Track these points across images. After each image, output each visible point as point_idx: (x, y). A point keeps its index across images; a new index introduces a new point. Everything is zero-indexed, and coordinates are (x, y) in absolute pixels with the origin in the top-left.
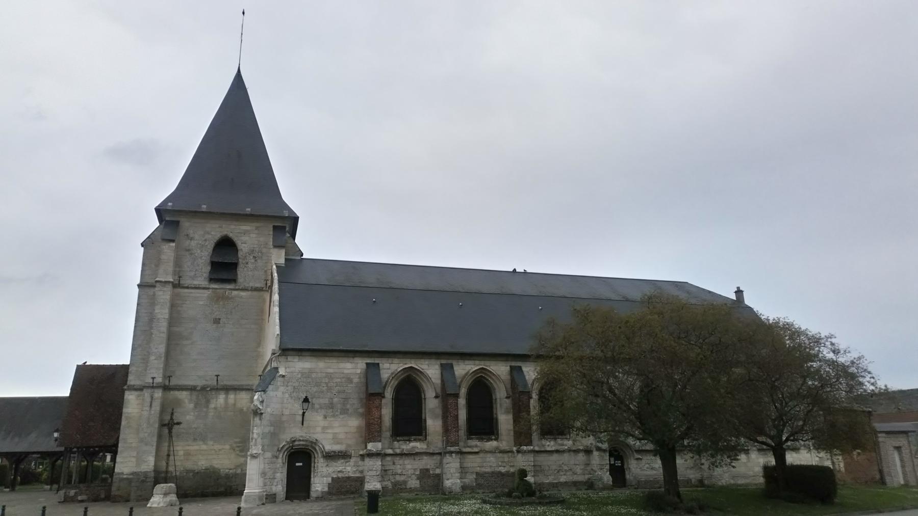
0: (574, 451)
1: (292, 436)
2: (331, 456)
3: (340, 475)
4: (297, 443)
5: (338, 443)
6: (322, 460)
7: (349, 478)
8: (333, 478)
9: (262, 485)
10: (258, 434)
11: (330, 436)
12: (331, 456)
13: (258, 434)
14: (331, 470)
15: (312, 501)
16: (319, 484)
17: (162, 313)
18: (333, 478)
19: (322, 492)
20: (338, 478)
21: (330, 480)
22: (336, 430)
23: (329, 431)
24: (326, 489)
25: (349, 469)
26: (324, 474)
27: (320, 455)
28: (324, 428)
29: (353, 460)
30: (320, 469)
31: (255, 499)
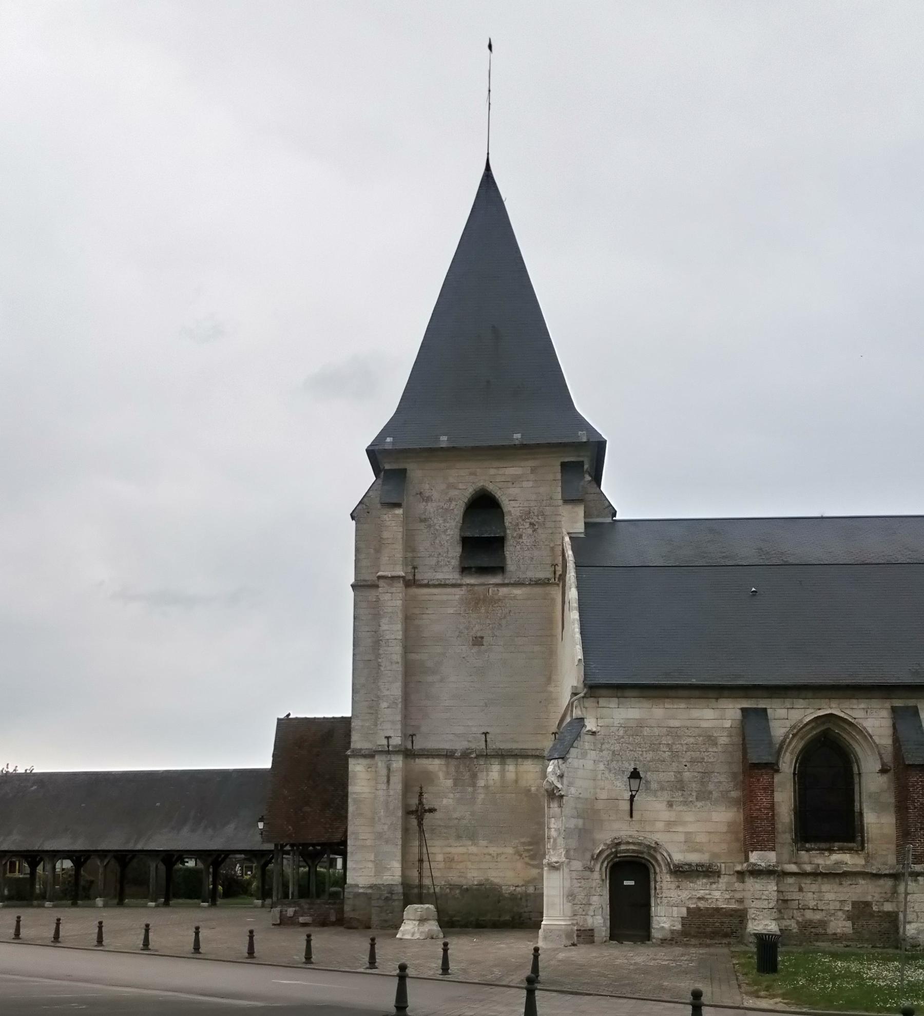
2: (683, 872)
3: (702, 904)
4: (623, 847)
6: (667, 878)
7: (718, 910)
8: (688, 909)
10: (558, 830)
11: (682, 838)
12: (683, 872)
14: (685, 895)
15: (654, 945)
16: (666, 916)
18: (688, 909)
20: (699, 909)
21: (684, 911)
24: (678, 927)
25: (717, 894)
27: (664, 870)
28: (669, 823)
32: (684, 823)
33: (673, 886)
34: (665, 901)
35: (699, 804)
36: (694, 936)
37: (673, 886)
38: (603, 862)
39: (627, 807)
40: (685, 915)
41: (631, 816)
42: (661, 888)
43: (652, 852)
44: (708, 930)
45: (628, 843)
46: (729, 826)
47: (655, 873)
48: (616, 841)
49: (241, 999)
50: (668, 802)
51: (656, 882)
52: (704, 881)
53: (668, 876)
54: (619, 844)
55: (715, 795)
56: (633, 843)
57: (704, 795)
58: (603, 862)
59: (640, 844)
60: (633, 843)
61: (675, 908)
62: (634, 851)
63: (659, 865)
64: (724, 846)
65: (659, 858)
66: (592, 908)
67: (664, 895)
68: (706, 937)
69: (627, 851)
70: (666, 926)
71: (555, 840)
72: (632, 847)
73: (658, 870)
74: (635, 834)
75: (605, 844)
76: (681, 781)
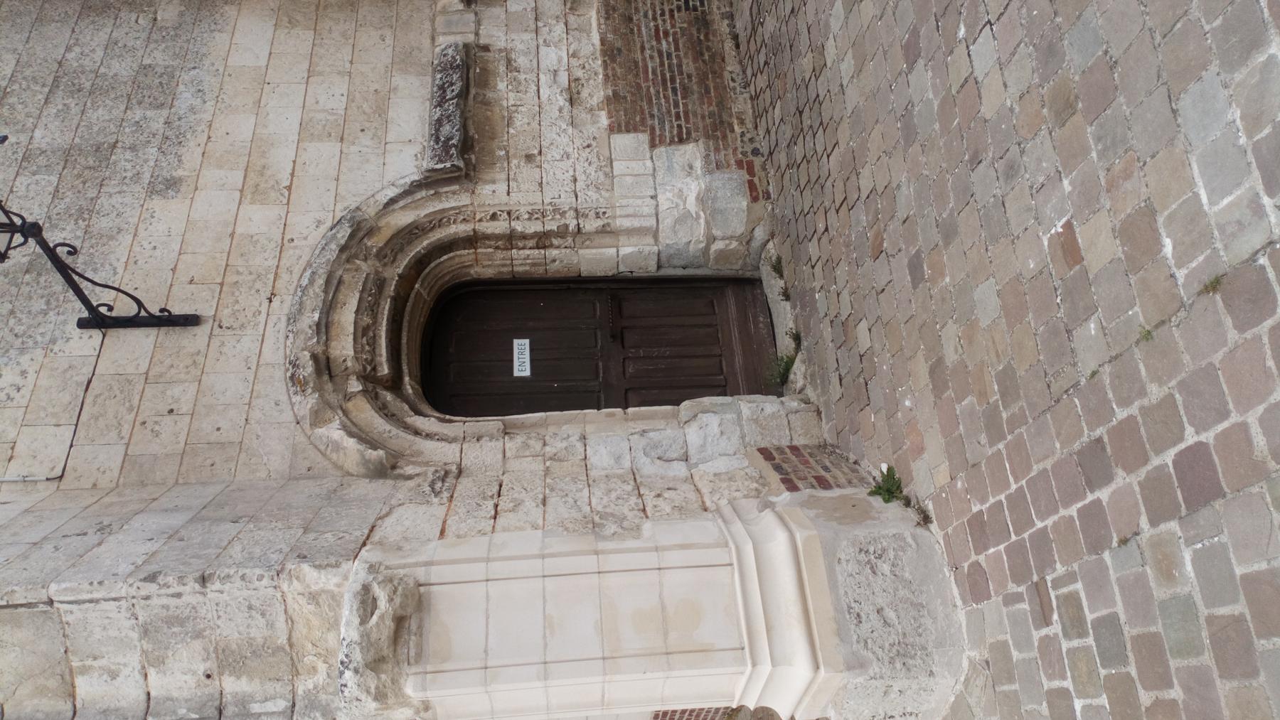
0: (64, 270)
1: (276, 385)
2: (466, 144)
3: (595, 92)
4: (344, 348)
5: (381, 110)
6: (492, 192)
7: (610, 53)
8: (614, 129)
9: (707, 528)
10: (156, 636)
11: (323, 153)
12: (466, 144)
13: (156, 636)
14: (559, 139)
15: (791, 230)
16: (653, 202)
17: (600, 285)
18: (614, 129)
19: (714, 166)
20: (614, 100)
21: (624, 142)
22: (283, 120)
23: (281, 159)
24: (692, 152)
25: (552, 57)
26: (588, 171)
27: (454, 199)
28: (253, 187)
29: (495, 34)
30: (558, 192)
31: (870, 557)
32: (259, 145)
33: (527, 174)
34: (590, 198)
35: (186, 98)
36: (721, 104)
37: (527, 174)
38: (417, 433)
39: (142, 339)
40: (644, 138)
41: (191, 321)
42: (537, 214)
43: (375, 242)
44: (689, 66)
45: (324, 327)
46: (292, 23)
47: (472, 240)
48: (308, 369)
49: (399, 343)
50: (152, 191)
51: (511, 240)
52: (502, 86)
53: (485, 190)
54: (325, 366)
55: (159, 57)
56: (329, 308)
57: (153, 88)
58: (417, 433)
59: (333, 286)
60: (329, 308)
61: (618, 167)
62: (368, 307)
63: (439, 220)
64: (368, 37)
65: (402, 218)
66: (648, 467)
67: (566, 201)
68: (718, 74)
69: (364, 333)
70: (693, 188)
71: (228, 659)
72: (346, 317)
73: (459, 229)
74: (282, 307)
75: (317, 419)
76: (68, 156)
